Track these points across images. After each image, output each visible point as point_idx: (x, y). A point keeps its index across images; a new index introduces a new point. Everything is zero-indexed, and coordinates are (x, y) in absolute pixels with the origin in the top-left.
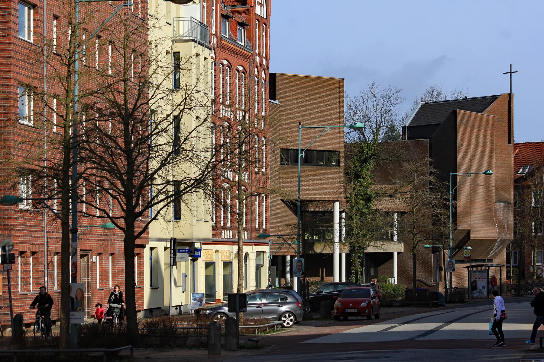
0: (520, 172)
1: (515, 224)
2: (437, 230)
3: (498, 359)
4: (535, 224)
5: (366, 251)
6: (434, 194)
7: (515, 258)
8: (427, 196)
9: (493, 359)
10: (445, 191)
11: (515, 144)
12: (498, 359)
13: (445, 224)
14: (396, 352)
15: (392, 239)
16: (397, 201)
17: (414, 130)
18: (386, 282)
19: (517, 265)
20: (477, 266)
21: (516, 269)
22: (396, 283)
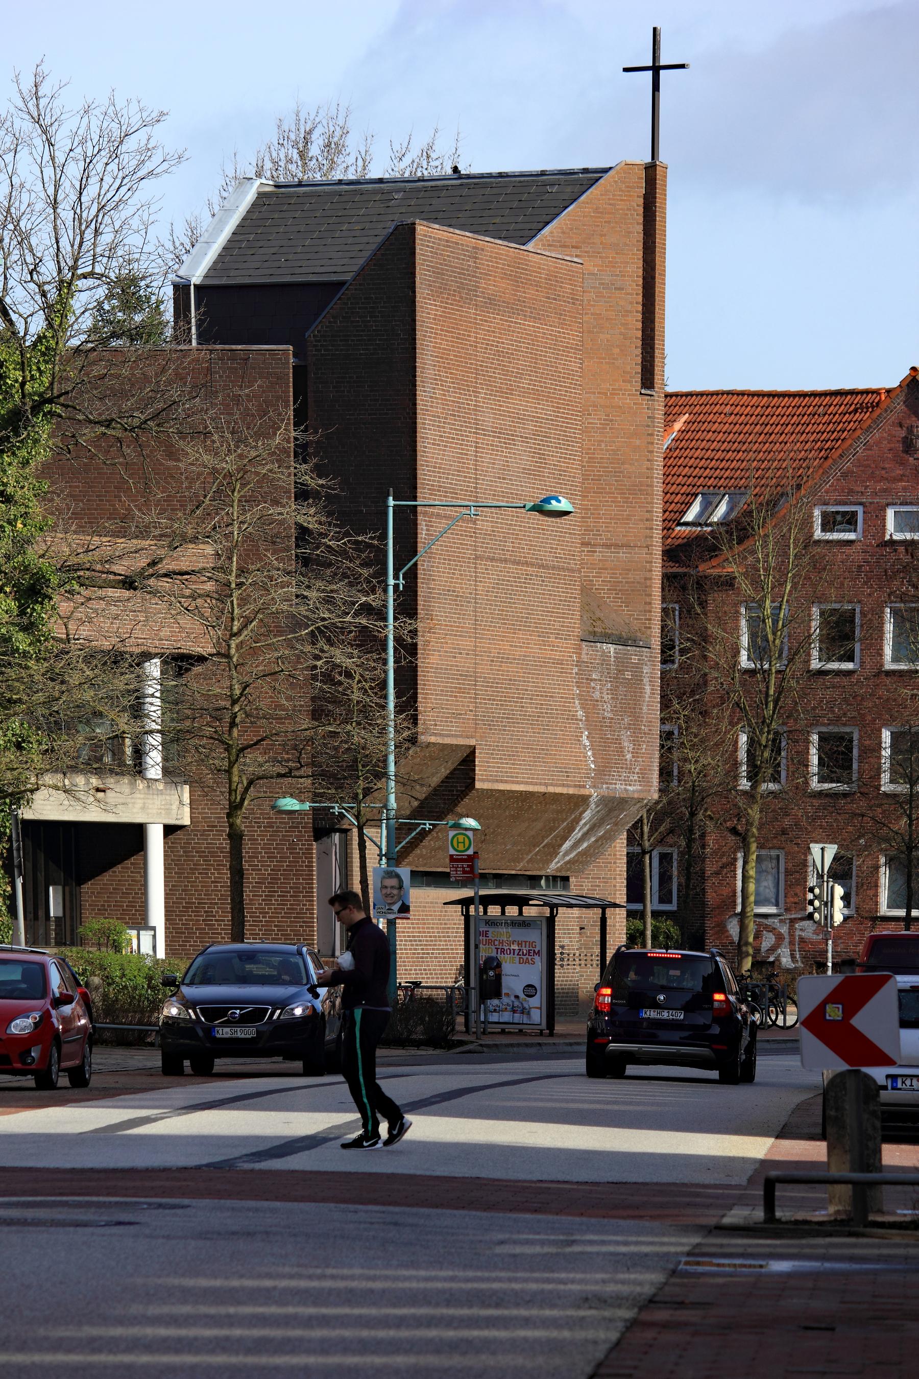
0: (690, 517)
1: (667, 736)
2: (329, 722)
3: (589, 1249)
4: (752, 742)
5: (27, 814)
6: (320, 584)
7: (665, 879)
8: (285, 593)
9: (568, 1250)
10: (365, 572)
11: (668, 396)
12: (589, 1249)
13: (368, 715)
14: (160, 1206)
15: (139, 769)
16: (156, 605)
17: (228, 306)
18: (117, 948)
19: (673, 907)
20: (503, 901)
21: (667, 925)
22: (161, 954)
